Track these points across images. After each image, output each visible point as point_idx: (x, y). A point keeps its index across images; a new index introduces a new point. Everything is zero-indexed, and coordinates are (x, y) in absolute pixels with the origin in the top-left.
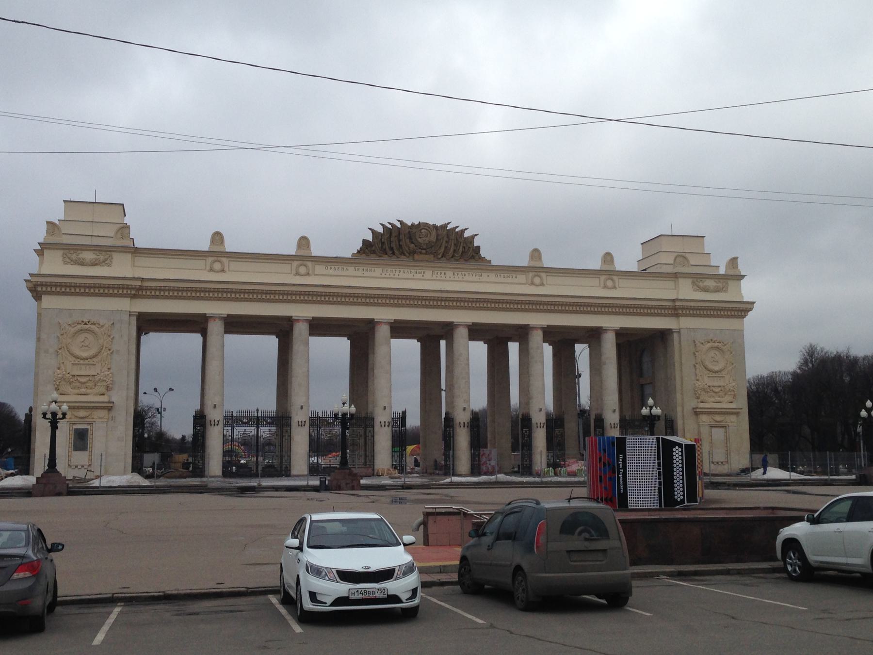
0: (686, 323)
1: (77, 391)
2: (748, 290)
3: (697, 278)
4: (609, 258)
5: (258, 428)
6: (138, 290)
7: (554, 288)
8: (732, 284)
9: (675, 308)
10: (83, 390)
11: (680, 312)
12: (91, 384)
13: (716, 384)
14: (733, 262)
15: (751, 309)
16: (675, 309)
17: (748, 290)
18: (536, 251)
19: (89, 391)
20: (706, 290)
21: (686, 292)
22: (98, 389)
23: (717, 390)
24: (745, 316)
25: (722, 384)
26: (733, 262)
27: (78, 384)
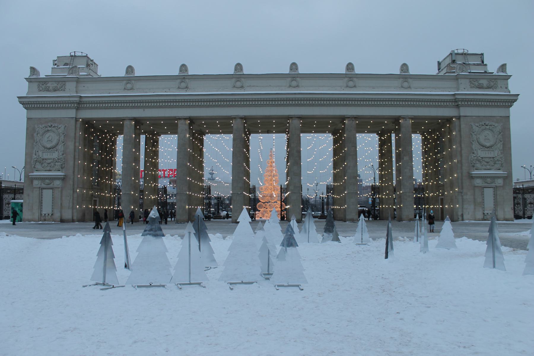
0: (465, 111)
1: (484, 167)
2: (513, 87)
3: (475, 80)
4: (350, 67)
5: (15, 195)
6: (80, 104)
7: (198, 90)
8: (500, 83)
9: (456, 101)
10: (488, 167)
11: (460, 103)
12: (492, 163)
13: (487, 155)
14: (503, 67)
15: (515, 100)
16: (456, 102)
17: (513, 87)
18: (183, 66)
19: (51, 169)
20: (480, 87)
21: (466, 90)
22: (497, 166)
23: (487, 160)
24: (511, 106)
25: (492, 155)
26: (503, 67)
27: (486, 164)
